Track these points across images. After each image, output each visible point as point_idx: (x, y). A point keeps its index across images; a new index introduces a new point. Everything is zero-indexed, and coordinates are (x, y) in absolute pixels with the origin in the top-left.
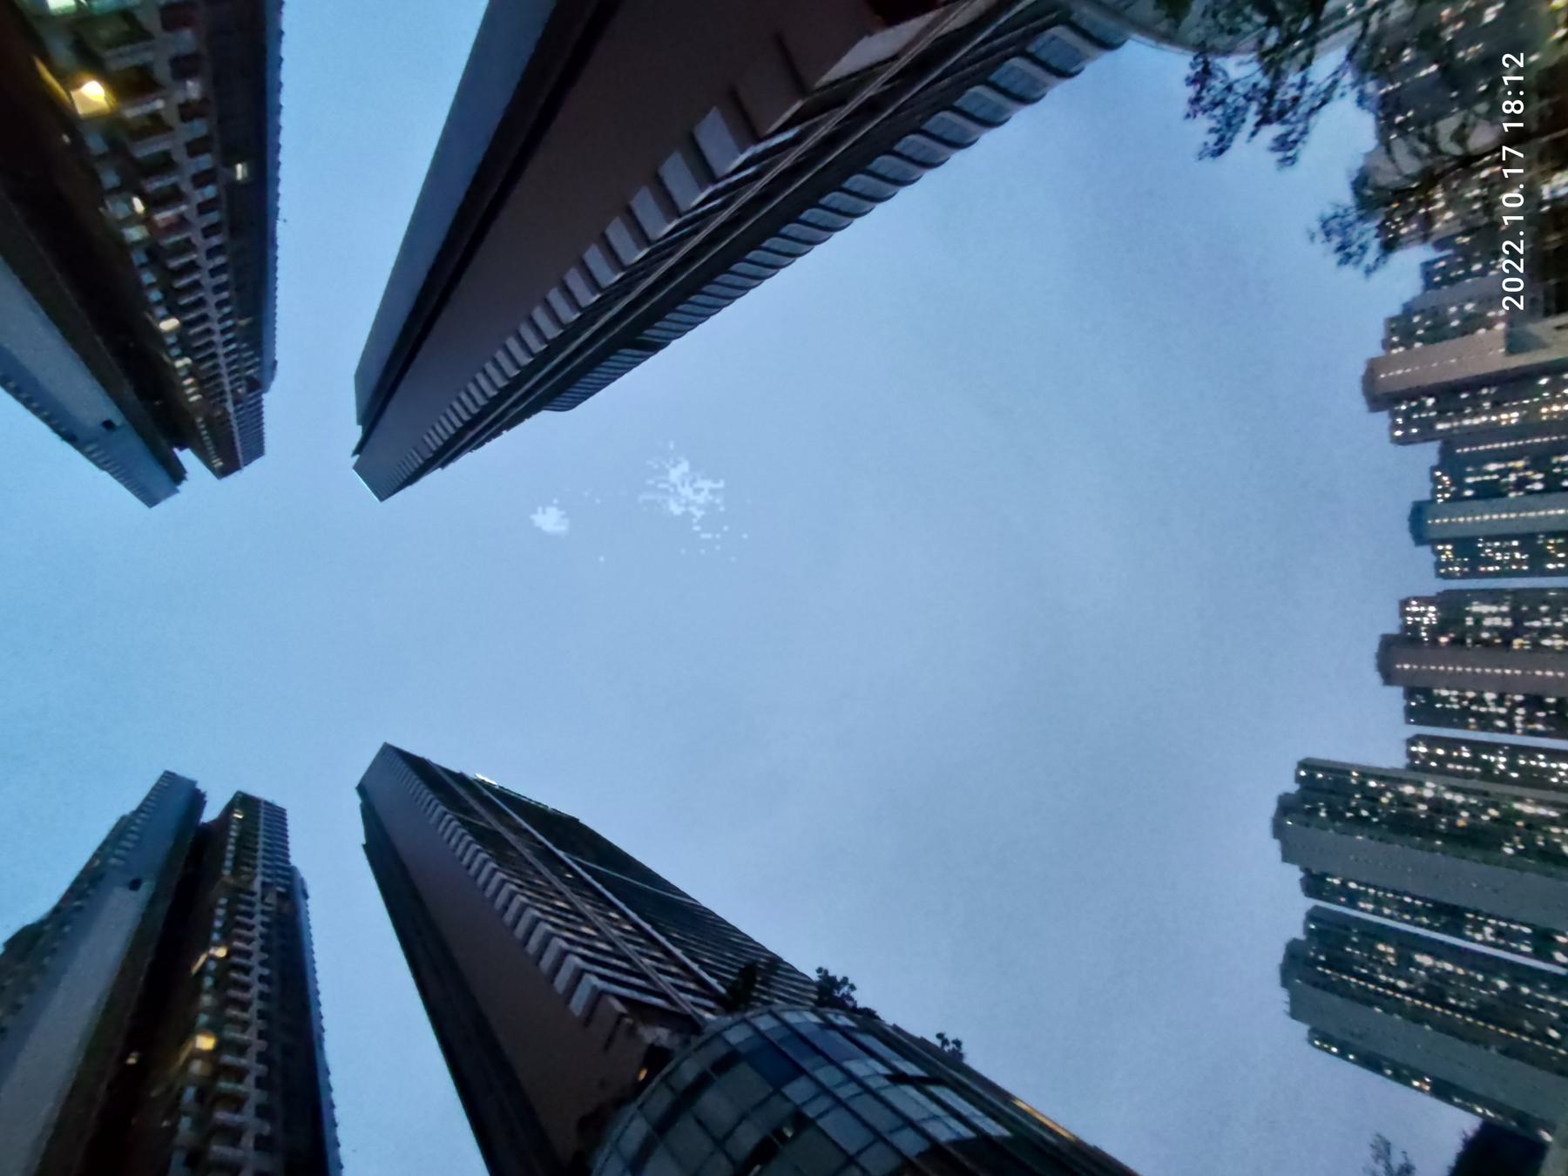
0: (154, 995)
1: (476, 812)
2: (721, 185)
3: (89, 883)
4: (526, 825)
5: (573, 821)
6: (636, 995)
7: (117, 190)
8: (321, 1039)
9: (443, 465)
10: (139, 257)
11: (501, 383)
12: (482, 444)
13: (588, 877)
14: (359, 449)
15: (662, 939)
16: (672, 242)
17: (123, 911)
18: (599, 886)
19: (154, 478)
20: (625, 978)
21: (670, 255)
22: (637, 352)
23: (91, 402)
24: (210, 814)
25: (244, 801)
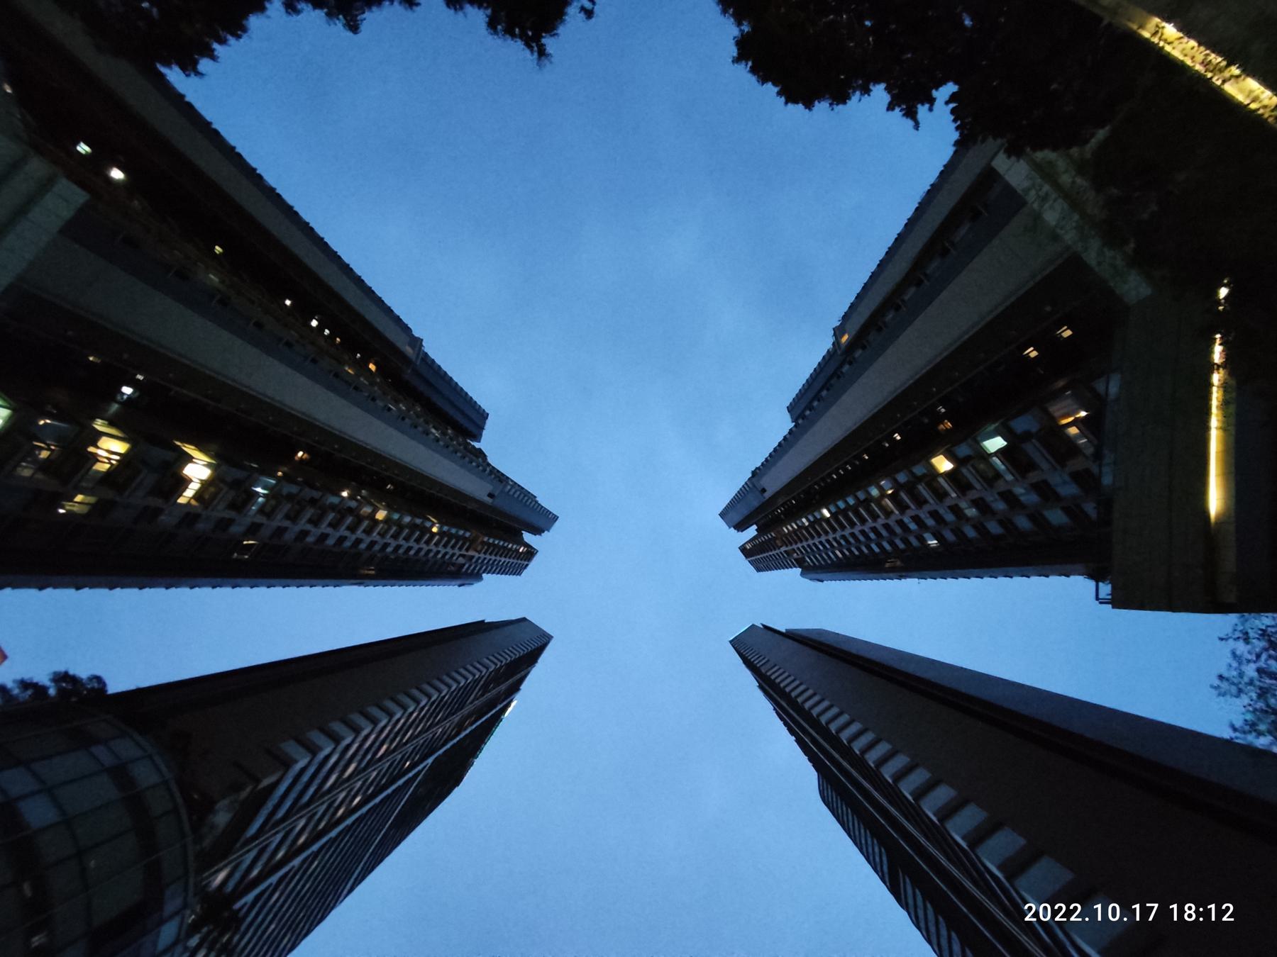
0: (419, 496)
1: (482, 695)
2: (1007, 885)
3: (501, 478)
4: (462, 735)
5: (457, 781)
6: (270, 805)
7: (895, 481)
8: (359, 584)
9: (761, 687)
10: (861, 495)
11: (833, 728)
12: (781, 718)
13: (401, 782)
14: (766, 627)
15: (315, 847)
16: (980, 876)
17: (476, 488)
18: (389, 791)
19: (736, 515)
20: (293, 795)
21: (949, 860)
22: (885, 868)
23: (773, 484)
24: (527, 537)
25: (531, 553)
